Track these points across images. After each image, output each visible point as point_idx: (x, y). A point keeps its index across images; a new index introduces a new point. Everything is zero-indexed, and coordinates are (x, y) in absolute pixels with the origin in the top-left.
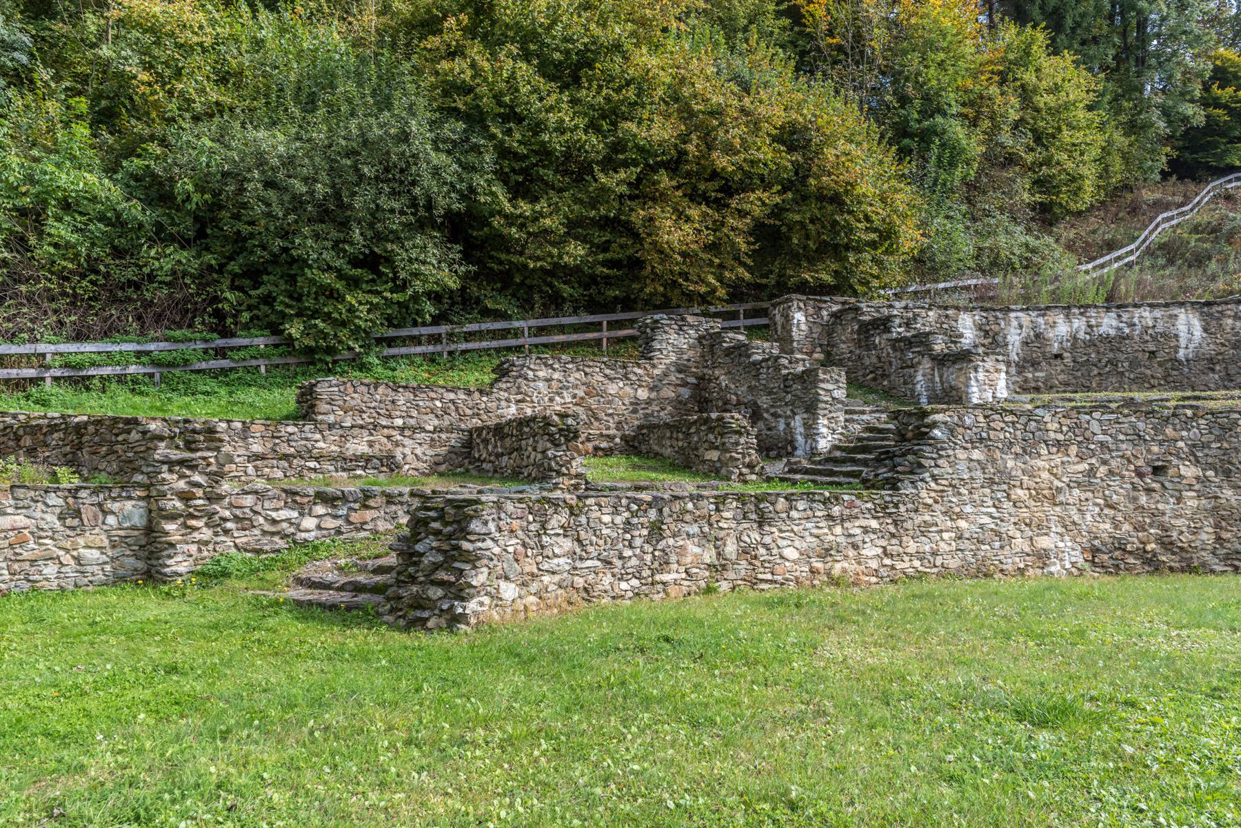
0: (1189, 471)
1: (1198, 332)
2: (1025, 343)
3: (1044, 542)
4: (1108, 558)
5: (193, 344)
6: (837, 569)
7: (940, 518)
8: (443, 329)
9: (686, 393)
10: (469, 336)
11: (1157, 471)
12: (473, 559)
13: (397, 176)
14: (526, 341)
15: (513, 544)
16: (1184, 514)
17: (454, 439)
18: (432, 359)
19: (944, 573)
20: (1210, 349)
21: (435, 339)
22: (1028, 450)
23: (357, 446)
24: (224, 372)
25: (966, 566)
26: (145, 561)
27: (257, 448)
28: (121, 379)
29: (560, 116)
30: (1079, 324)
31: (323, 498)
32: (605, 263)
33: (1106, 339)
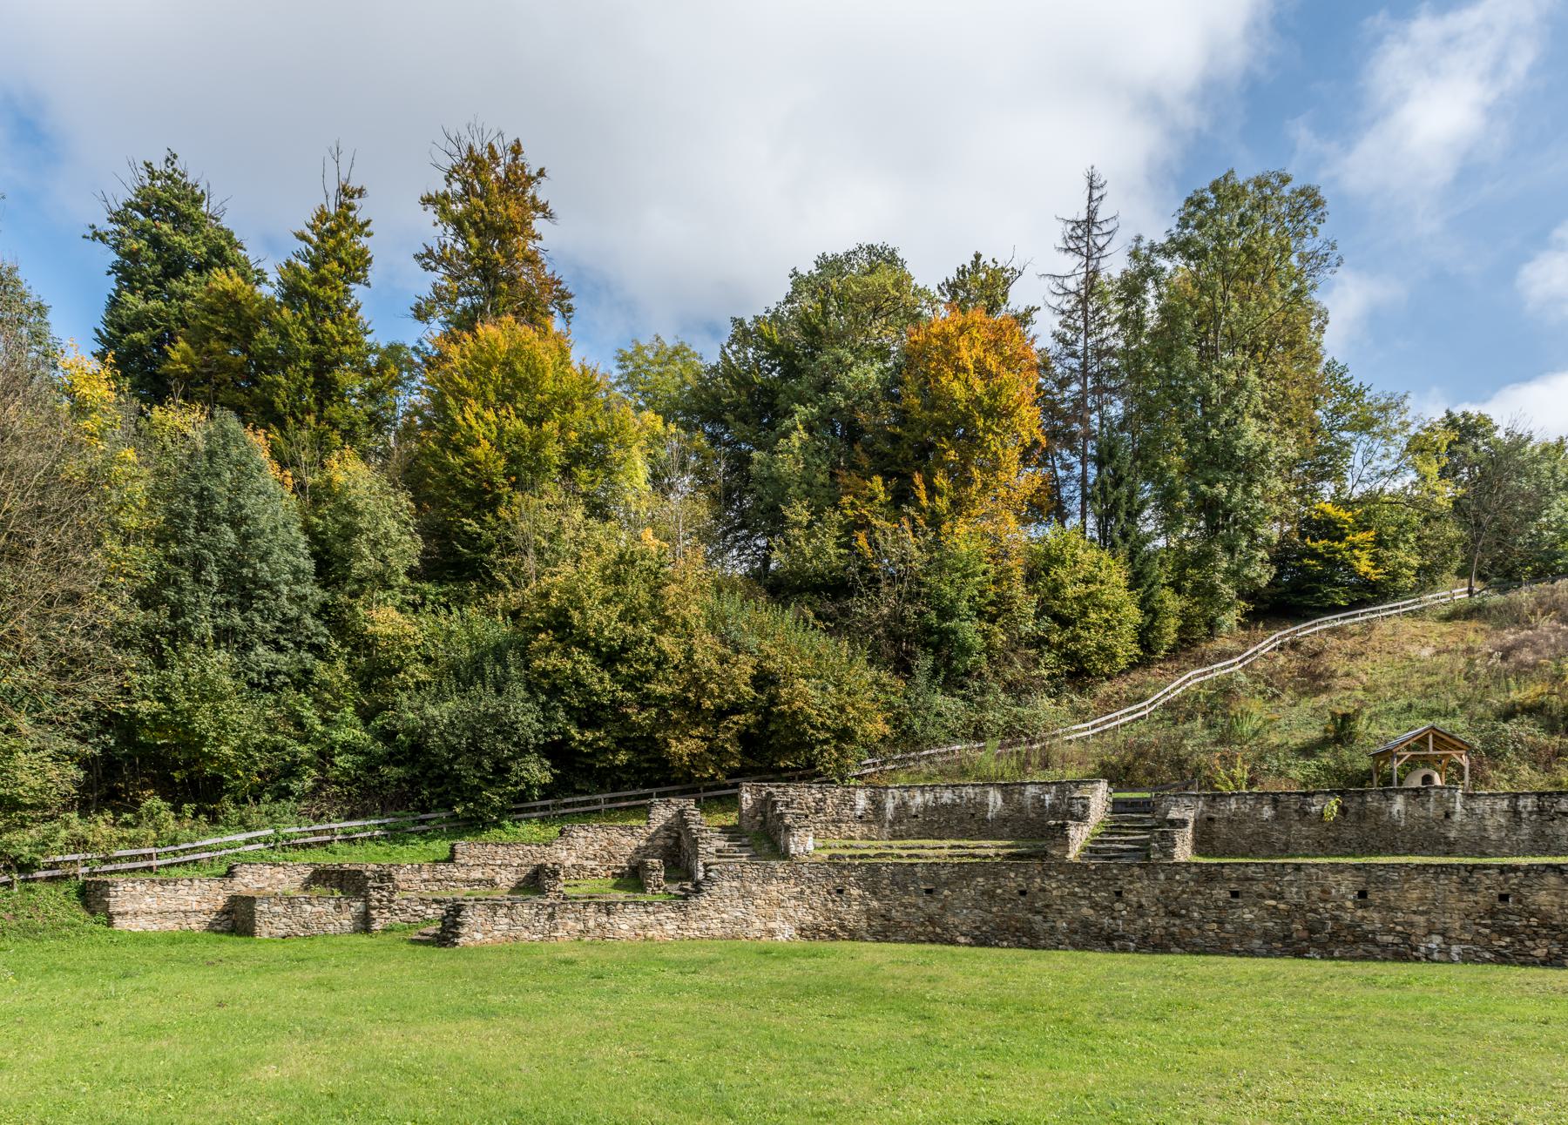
0: (855, 892)
1: (1000, 802)
2: (896, 808)
3: (772, 925)
5: (406, 818)
6: (650, 934)
7: (712, 913)
8: (550, 802)
9: (670, 842)
10: (566, 805)
11: (840, 892)
12: (462, 924)
13: (506, 730)
14: (603, 806)
15: (480, 920)
16: (852, 913)
17: (529, 870)
19: (713, 937)
20: (1006, 813)
21: (546, 808)
22: (767, 880)
23: (476, 874)
24: (424, 832)
25: (726, 934)
26: (364, 924)
27: (425, 876)
28: (371, 838)
29: (602, 684)
30: (929, 796)
31: (436, 901)
32: (648, 761)
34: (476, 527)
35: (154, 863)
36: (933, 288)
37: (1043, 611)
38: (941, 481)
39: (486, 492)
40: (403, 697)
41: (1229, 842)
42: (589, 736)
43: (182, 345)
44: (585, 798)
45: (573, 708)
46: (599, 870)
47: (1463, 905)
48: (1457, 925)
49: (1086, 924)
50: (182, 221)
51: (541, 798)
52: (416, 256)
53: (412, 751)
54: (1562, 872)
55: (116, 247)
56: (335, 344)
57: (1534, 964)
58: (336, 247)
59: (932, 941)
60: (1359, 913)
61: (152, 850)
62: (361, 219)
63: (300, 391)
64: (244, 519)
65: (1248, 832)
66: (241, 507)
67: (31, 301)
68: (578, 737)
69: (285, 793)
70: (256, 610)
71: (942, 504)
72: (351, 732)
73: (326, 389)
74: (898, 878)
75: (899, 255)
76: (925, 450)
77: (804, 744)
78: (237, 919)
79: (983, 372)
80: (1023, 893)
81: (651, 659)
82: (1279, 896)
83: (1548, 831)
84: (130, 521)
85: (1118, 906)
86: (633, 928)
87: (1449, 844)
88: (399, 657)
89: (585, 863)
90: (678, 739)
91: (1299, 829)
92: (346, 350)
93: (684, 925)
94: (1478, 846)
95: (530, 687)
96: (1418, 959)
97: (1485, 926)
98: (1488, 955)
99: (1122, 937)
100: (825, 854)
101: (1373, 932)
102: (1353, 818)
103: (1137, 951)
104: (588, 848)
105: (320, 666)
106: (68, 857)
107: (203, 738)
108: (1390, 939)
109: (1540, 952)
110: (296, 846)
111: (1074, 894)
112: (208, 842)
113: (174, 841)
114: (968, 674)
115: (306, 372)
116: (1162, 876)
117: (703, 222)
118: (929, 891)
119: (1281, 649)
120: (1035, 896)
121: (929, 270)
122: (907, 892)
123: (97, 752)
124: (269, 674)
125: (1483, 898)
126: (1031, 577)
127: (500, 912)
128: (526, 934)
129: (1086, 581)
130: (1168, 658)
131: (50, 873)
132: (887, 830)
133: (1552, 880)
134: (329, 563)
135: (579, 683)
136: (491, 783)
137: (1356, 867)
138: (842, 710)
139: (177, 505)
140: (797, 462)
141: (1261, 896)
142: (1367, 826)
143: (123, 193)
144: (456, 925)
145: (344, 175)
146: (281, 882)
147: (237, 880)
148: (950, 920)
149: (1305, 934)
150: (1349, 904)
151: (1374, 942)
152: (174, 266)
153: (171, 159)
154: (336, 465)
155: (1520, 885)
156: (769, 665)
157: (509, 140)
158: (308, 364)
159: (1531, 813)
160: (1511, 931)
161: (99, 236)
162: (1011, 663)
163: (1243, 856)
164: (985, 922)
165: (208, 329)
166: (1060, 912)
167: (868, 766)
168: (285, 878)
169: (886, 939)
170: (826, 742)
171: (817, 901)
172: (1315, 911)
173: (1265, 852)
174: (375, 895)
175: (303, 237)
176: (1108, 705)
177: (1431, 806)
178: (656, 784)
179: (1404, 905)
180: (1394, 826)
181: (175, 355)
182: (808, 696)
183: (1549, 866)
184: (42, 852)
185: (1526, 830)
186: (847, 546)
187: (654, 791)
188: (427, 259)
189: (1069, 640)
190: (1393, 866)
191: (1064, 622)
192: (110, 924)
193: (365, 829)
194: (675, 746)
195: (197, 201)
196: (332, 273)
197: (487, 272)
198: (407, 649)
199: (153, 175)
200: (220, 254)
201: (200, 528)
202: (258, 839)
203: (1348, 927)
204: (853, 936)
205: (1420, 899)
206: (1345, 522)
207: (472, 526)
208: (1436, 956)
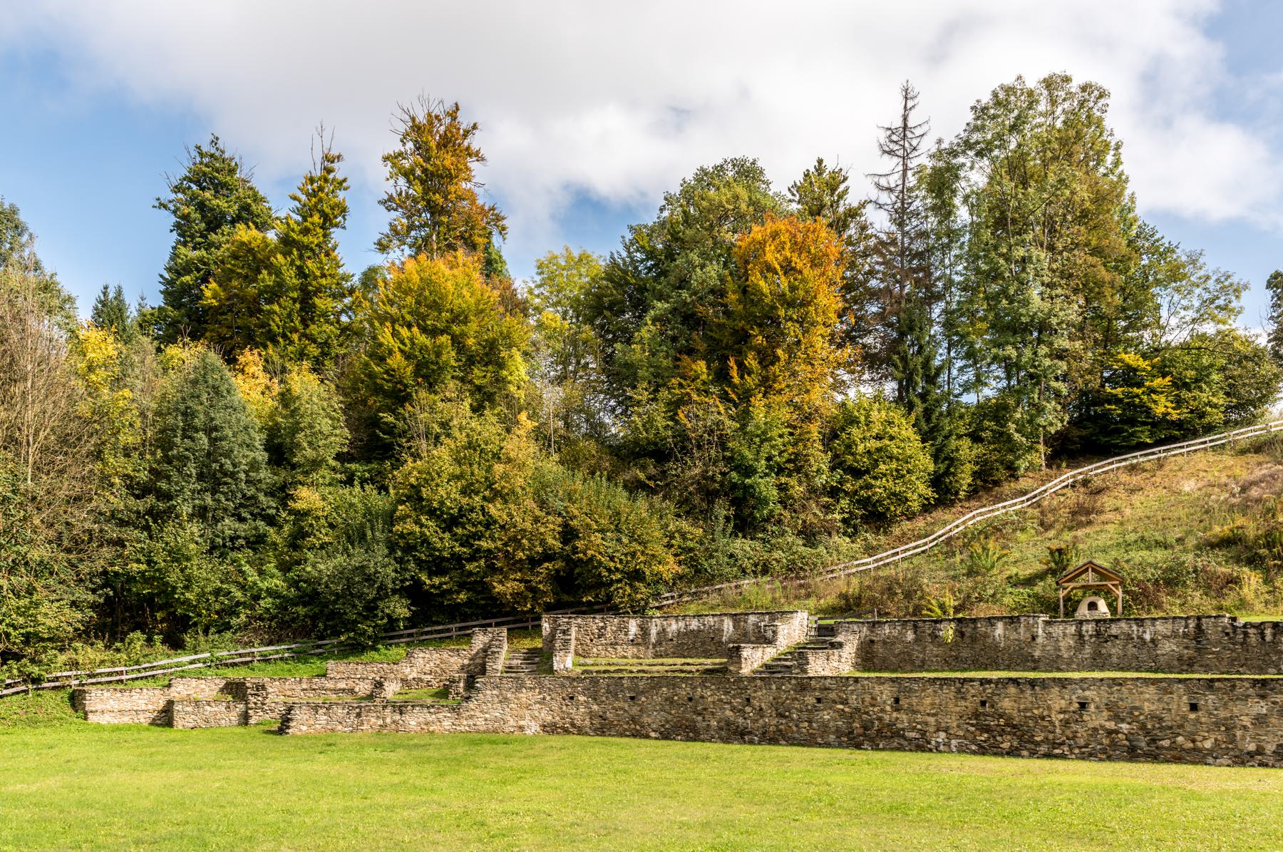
0: (582, 698)
3: (522, 723)
4: (550, 729)
7: (478, 714)
8: (414, 631)
12: (292, 719)
14: (454, 633)
15: (306, 717)
16: (579, 715)
18: (408, 644)
21: (411, 635)
22: (518, 689)
23: (342, 685)
26: (245, 719)
27: (304, 686)
29: (445, 543)
30: (682, 624)
33: (692, 631)
34: (391, 419)
35: (124, 677)
36: (785, 192)
37: (836, 464)
38: (751, 361)
39: (400, 391)
40: (310, 555)
41: (884, 660)
42: (437, 581)
43: (213, 285)
44: (440, 627)
45: (422, 561)
46: (434, 682)
47: (958, 709)
48: (955, 724)
49: (728, 723)
50: (220, 188)
51: (406, 628)
52: (379, 202)
53: (310, 595)
54: (1018, 684)
55: (174, 212)
56: (315, 278)
57: (1002, 755)
58: (323, 203)
59: (634, 736)
60: (895, 715)
61: (123, 669)
62: (340, 177)
63: (289, 315)
64: (216, 429)
65: (897, 651)
66: (212, 419)
67: (64, 294)
68: (428, 582)
69: (228, 627)
70: (222, 493)
71: (750, 381)
72: (277, 582)
73: (307, 311)
74: (611, 688)
75: (759, 164)
76: (744, 337)
77: (600, 584)
78: (165, 718)
79: (788, 269)
80: (690, 699)
81: (480, 523)
82: (844, 702)
83: (1104, 651)
84: (127, 438)
85: (748, 709)
86: (419, 724)
87: (1034, 661)
88: (311, 525)
89: (423, 677)
90: (501, 582)
91: (932, 649)
92: (323, 282)
93: (457, 722)
94: (1055, 664)
95: (392, 547)
96: (931, 750)
97: (972, 725)
98: (974, 747)
99: (750, 733)
100: (579, 669)
101: (903, 729)
102: (968, 641)
103: (759, 743)
104: (427, 663)
105: (272, 530)
106: (65, 674)
107: (174, 588)
108: (913, 735)
109: (1006, 745)
110: (226, 665)
111: (721, 700)
112: (162, 663)
113: (137, 663)
114: (767, 520)
115: (294, 300)
116: (774, 687)
117: (582, 164)
118: (632, 698)
119: (1073, 486)
120: (697, 702)
121: (782, 177)
122: (617, 699)
123: (102, 601)
124: (232, 539)
125: (970, 704)
126: (831, 437)
127: (320, 711)
128: (340, 727)
129: (878, 437)
130: (968, 498)
131: (53, 684)
132: (651, 651)
133: (1012, 690)
134: (279, 451)
135: (425, 541)
136: (366, 618)
137: (892, 680)
138: (633, 555)
139: (170, 420)
140: (644, 351)
141: (835, 702)
142: (978, 647)
143: (180, 171)
144: (289, 720)
145: (327, 146)
146: (203, 690)
147: (172, 689)
148: (646, 720)
149: (861, 731)
150: (888, 708)
151: (904, 737)
152: (215, 221)
153: (215, 142)
154: (296, 378)
155: (993, 693)
156: (574, 523)
157: (449, 106)
158: (295, 295)
159: (1091, 636)
160: (987, 729)
161: (163, 206)
162: (396, 571)
163: (1008, 668)
164: (667, 722)
165: (232, 271)
166: (713, 713)
167: (667, 598)
168: (208, 688)
169: (603, 734)
170: (619, 581)
171: (555, 706)
172: (867, 713)
173: (909, 668)
174: (252, 699)
175: (295, 198)
176: (903, 539)
177: (1022, 630)
178: (494, 616)
179: (922, 709)
180: (996, 647)
181: (208, 293)
182: (598, 546)
183: (1010, 679)
184: (46, 671)
185: (1088, 650)
186: (672, 418)
187: (493, 621)
188: (389, 203)
189: (861, 488)
190: (915, 679)
191: (857, 473)
192: (86, 719)
193: (277, 652)
194: (499, 588)
195: (232, 171)
196: (313, 224)
197: (432, 208)
198: (317, 518)
199: (201, 155)
200: (246, 214)
201: (184, 436)
202: (199, 660)
203: (888, 725)
204: (581, 731)
205: (932, 704)
206: (1144, 370)
207: (389, 418)
208: (942, 748)
